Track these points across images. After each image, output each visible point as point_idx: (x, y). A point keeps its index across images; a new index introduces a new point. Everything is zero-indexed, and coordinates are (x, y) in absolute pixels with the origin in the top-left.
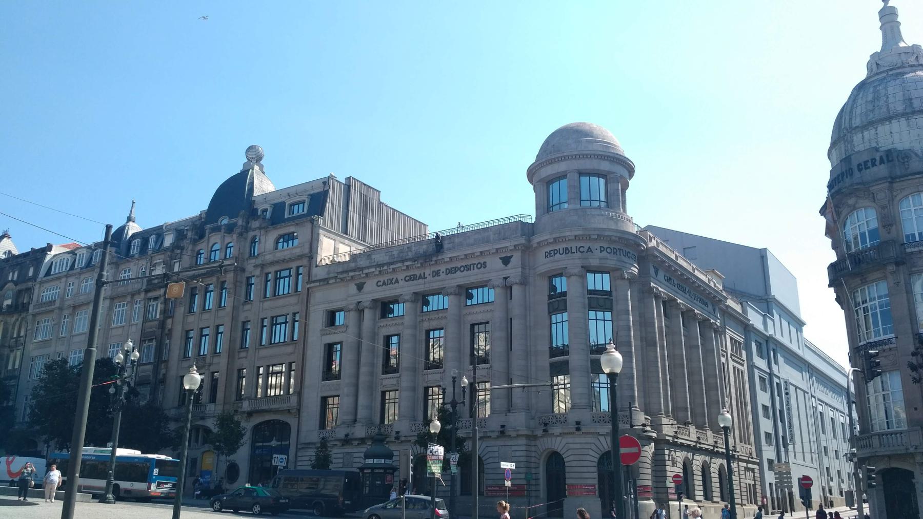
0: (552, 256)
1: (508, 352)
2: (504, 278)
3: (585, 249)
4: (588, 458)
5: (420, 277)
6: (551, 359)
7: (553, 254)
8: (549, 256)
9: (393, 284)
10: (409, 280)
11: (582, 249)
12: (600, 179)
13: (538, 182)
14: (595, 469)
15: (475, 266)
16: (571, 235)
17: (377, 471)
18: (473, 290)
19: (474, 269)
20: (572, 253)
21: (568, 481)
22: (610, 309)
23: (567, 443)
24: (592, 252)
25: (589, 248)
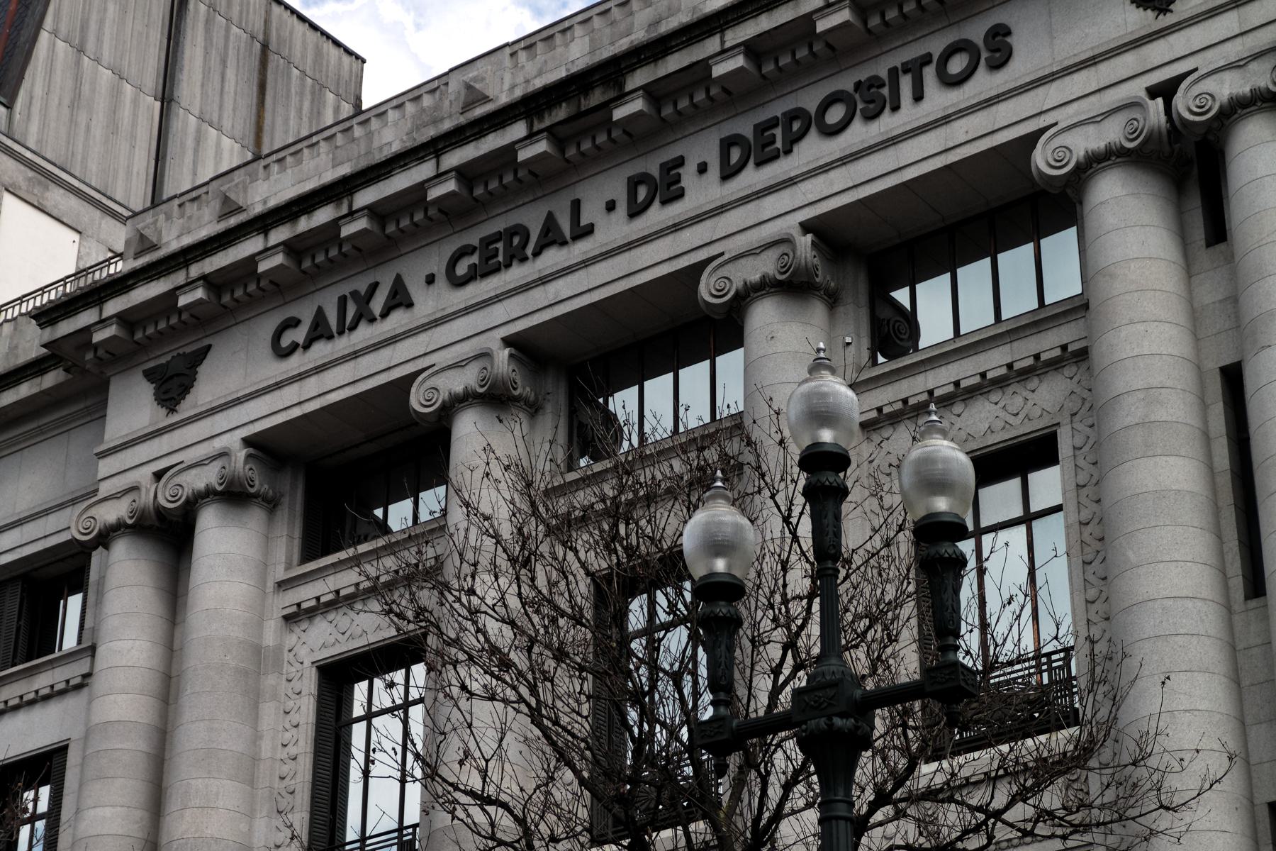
2: (1153, 92)
5: (551, 237)
9: (372, 320)
10: (474, 275)
15: (929, 73)
19: (918, 97)
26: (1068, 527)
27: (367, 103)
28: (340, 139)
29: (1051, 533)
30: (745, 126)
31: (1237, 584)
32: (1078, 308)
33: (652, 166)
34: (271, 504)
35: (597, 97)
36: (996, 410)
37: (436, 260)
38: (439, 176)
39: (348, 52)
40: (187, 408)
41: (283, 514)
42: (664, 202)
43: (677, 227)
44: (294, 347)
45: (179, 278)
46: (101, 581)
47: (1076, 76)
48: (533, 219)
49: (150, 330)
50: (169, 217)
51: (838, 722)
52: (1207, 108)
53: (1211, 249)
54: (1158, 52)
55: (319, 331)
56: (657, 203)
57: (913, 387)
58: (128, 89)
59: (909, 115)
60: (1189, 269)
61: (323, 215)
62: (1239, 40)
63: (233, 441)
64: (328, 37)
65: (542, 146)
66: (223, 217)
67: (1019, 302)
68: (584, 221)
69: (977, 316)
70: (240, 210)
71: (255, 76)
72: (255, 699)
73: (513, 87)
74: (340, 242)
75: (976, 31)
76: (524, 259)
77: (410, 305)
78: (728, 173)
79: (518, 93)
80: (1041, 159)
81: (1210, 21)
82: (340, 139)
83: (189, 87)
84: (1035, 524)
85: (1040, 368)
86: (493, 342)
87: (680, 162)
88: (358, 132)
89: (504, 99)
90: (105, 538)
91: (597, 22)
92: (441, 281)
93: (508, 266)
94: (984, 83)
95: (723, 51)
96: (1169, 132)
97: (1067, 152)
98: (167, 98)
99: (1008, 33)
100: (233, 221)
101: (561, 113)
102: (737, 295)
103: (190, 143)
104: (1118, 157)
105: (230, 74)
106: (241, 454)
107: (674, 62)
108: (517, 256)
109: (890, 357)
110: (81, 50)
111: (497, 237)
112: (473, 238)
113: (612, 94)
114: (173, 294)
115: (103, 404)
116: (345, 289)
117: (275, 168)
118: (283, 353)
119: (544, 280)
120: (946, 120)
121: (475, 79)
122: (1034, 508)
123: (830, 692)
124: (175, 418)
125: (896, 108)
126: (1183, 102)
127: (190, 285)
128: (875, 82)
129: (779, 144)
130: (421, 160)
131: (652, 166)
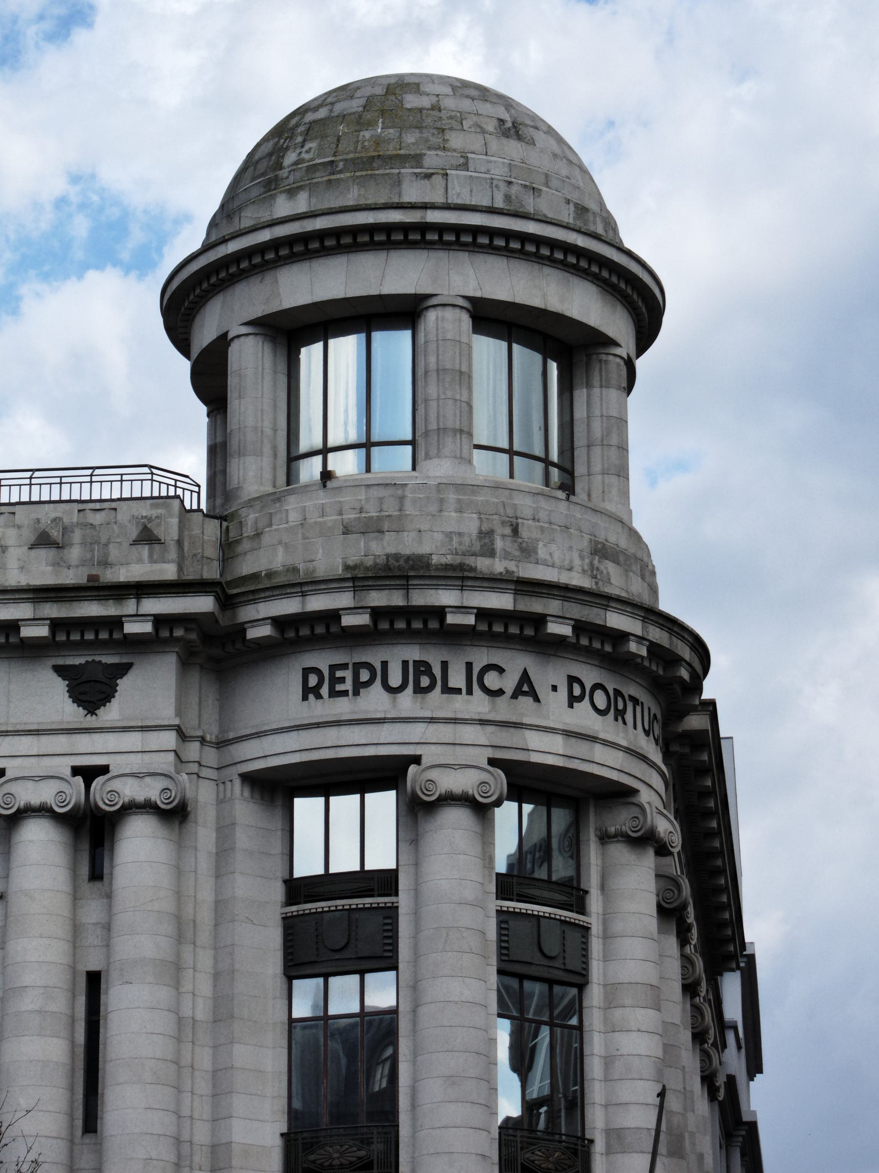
0: (345, 693)
2: (76, 771)
3: (509, 683)
7: (348, 686)
8: (325, 691)
11: (492, 680)
12: (515, 347)
13: (247, 324)
16: (461, 609)
20: (448, 690)
24: (537, 699)
25: (525, 677)
31: (79, 1123)
47: (23, 738)
52: (114, 802)
53: (92, 884)
54: (83, 742)
60: (76, 897)
62: (140, 755)
81: (123, 734)
96: (85, 809)
97: (13, 799)
104: (47, 812)
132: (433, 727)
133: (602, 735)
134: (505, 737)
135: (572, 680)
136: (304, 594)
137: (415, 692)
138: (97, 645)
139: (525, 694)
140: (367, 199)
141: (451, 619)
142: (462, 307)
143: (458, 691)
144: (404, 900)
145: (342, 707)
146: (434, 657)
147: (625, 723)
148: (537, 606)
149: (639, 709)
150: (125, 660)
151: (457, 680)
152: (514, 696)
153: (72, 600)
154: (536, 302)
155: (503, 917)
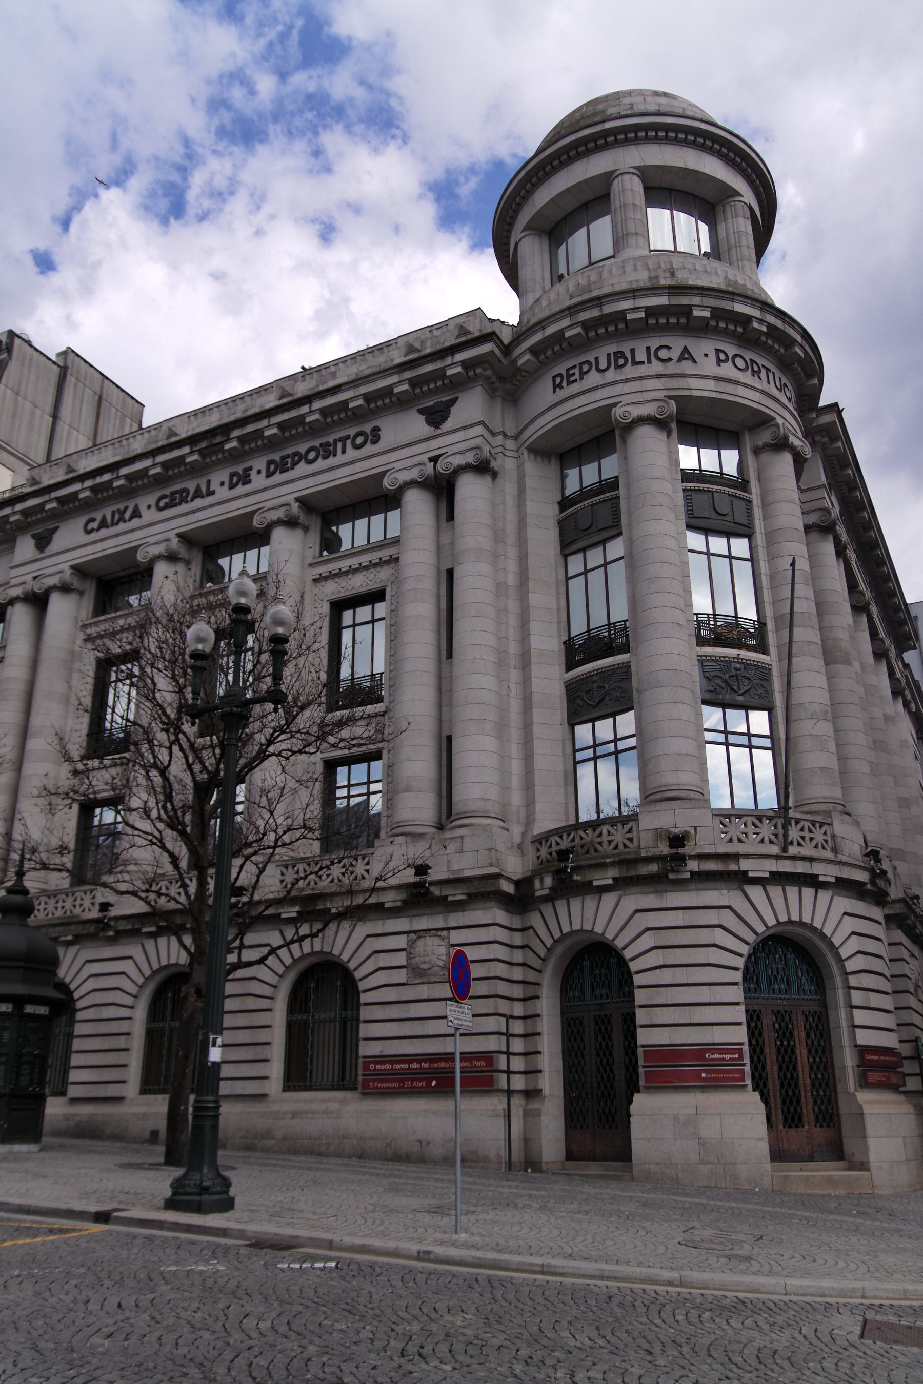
1: (439, 662)
2: (431, 459)
3: (675, 354)
4: (715, 956)
5: (198, 494)
6: (571, 673)
7: (577, 376)
8: (564, 384)
9: (125, 521)
10: (167, 506)
11: (663, 354)
13: (523, 231)
14: (736, 994)
15: (349, 442)
17: (29, 1009)
18: (340, 527)
19: (344, 452)
20: (635, 363)
21: (644, 1037)
22: (746, 532)
23: (637, 911)
25: (686, 349)
26: (386, 626)
27: (145, 425)
28: (117, 445)
29: (380, 627)
30: (276, 457)
31: (444, 652)
32: (396, 541)
33: (240, 469)
34: (81, 593)
35: (219, 439)
36: (364, 578)
37: (151, 499)
38: (154, 465)
39: (138, 402)
40: (48, 551)
41: (86, 597)
42: (243, 484)
43: (247, 495)
44: (92, 530)
45: (46, 498)
46: (10, 620)
48: (191, 485)
49: (140, 483)
50: (45, 471)
51: (235, 709)
54: (434, 444)
55: (103, 524)
56: (240, 485)
57: (334, 567)
58: (38, 412)
59: (340, 459)
60: (438, 531)
61: (107, 477)
63: (66, 567)
64: (129, 395)
65: (196, 457)
66: (68, 473)
67: (377, 536)
68: (211, 489)
69: (361, 541)
70: (74, 471)
71: (95, 411)
72: (70, 671)
73: (187, 431)
74: (186, 464)
75: (367, 428)
76: (187, 502)
77: (140, 517)
78: (269, 475)
79: (190, 433)
80: (386, 483)
82: (117, 445)
83: (66, 412)
84: (376, 624)
85: (381, 563)
86: (172, 535)
87: (251, 468)
88: (124, 443)
89: (184, 435)
90: (12, 602)
91: (223, 407)
92: (153, 509)
93: (180, 504)
94: (369, 449)
95: (311, 412)
98: (55, 416)
99: (380, 430)
100: (71, 475)
101: (204, 444)
102: (268, 525)
103: (65, 436)
105: (84, 408)
106: (68, 572)
107: (250, 428)
108: (184, 500)
109: (330, 552)
110: (18, 394)
111: (177, 492)
112: (167, 491)
113: (224, 439)
114: (43, 505)
115: (14, 547)
116: (115, 508)
117: (90, 454)
118: (88, 532)
119: (193, 512)
120: (353, 462)
121: (173, 426)
122: (357, 622)
123: (232, 698)
124: (43, 555)
125: (335, 455)
126: (439, 466)
127: (51, 501)
128: (328, 444)
129: (289, 465)
130: (147, 458)
131: (240, 469)
132: (627, 385)
133: (741, 381)
134: (674, 383)
135: (718, 351)
136: (543, 328)
137: (616, 368)
138: (437, 391)
139: (687, 359)
140: (903, 743)
141: (629, 317)
142: (634, 174)
143: (643, 363)
144: (622, 492)
145: (575, 388)
146: (626, 348)
147: (760, 378)
148: (685, 300)
149: (771, 375)
150: (454, 396)
151: (641, 356)
152: (679, 361)
153: (418, 366)
154: (681, 164)
155: (688, 493)
